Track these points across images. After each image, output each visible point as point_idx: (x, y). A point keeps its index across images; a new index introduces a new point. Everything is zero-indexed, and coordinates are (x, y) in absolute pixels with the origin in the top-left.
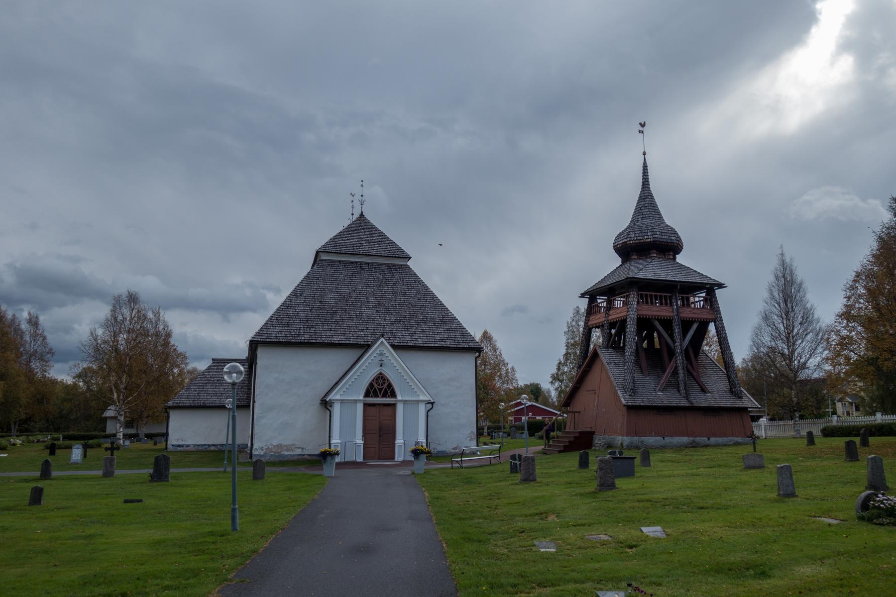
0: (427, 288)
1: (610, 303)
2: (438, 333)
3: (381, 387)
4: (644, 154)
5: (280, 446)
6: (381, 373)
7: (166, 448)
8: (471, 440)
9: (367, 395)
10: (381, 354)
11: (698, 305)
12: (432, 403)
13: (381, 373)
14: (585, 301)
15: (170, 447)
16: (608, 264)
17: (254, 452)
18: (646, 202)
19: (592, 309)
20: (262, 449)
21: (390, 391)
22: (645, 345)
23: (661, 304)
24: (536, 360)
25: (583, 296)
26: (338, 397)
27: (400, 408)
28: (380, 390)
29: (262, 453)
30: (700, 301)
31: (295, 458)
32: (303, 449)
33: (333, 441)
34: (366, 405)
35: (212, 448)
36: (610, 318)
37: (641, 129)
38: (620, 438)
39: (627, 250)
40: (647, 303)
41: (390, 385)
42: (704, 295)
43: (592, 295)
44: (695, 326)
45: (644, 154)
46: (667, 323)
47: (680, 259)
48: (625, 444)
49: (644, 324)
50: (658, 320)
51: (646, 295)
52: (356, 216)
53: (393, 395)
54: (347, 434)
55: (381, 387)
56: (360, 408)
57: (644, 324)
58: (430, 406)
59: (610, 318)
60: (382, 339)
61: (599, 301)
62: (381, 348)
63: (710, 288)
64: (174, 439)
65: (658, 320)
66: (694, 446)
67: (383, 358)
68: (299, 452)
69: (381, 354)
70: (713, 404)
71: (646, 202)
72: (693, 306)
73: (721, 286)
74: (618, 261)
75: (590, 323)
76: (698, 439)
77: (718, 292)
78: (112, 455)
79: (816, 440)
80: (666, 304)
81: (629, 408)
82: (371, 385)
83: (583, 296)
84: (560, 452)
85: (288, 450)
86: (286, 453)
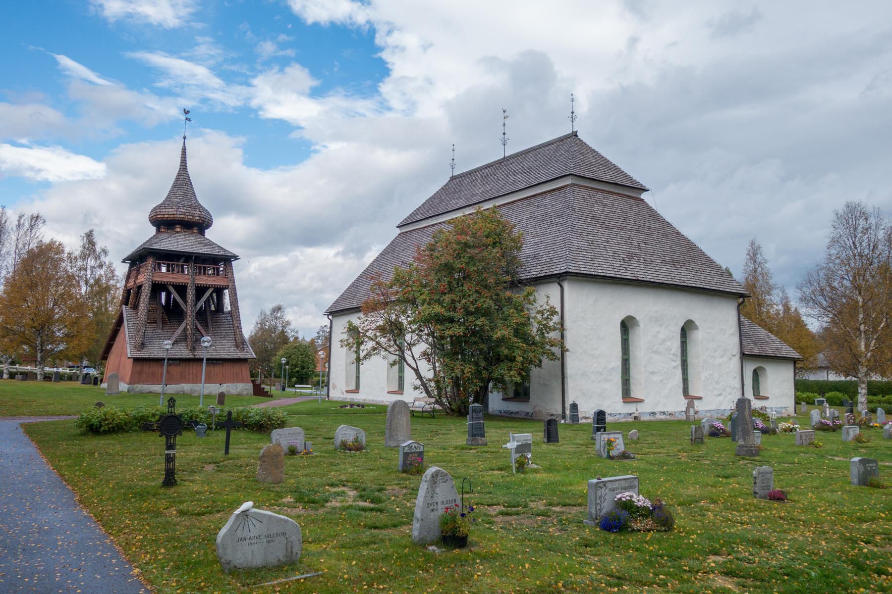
0: (361, 276)
16: (142, 233)
18: (183, 180)
25: (124, 261)
37: (188, 116)
39: (163, 223)
40: (200, 273)
46: (181, 289)
47: (209, 234)
49: (157, 288)
50: (173, 285)
56: (206, 385)
57: (157, 288)
63: (227, 259)
65: (173, 285)
70: (152, 356)
71: (183, 180)
73: (236, 258)
74: (153, 230)
79: (561, 433)
81: (136, 360)
83: (124, 261)
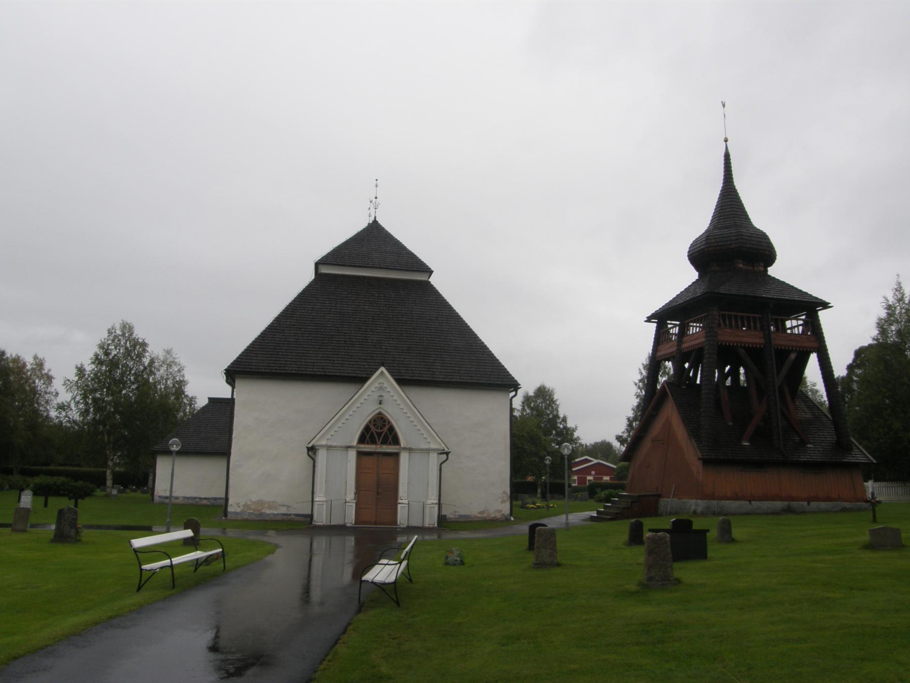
1: (683, 329)
2: (462, 362)
3: (379, 433)
4: (726, 141)
5: (261, 502)
6: (380, 413)
7: (153, 500)
8: (503, 502)
9: (362, 440)
10: (381, 388)
11: (796, 331)
12: (447, 454)
13: (380, 413)
14: (653, 326)
15: (156, 499)
17: (230, 509)
19: (661, 336)
20: (238, 504)
21: (391, 437)
22: (728, 382)
23: (749, 328)
24: (601, 398)
25: (649, 320)
26: (324, 442)
27: (404, 457)
28: (379, 434)
29: (239, 510)
30: (798, 326)
31: (279, 518)
32: (288, 507)
33: (316, 499)
34: (360, 454)
35: (204, 502)
36: (684, 346)
38: (693, 501)
41: (392, 429)
42: (803, 317)
43: (661, 317)
44: (793, 356)
45: (726, 141)
48: (699, 509)
50: (745, 348)
51: (730, 316)
52: (372, 219)
53: (396, 441)
54: (336, 490)
55: (379, 433)
56: (352, 455)
58: (445, 456)
59: (684, 346)
60: (382, 369)
61: (669, 326)
62: (381, 380)
64: (161, 487)
66: (789, 510)
67: (382, 392)
68: (283, 510)
69: (381, 388)
71: (730, 204)
72: (789, 331)
75: (659, 354)
76: (794, 504)
77: (823, 315)
78: (76, 505)
80: (755, 328)
82: (367, 428)
83: (649, 320)
84: (611, 519)
85: (270, 508)
86: (268, 512)
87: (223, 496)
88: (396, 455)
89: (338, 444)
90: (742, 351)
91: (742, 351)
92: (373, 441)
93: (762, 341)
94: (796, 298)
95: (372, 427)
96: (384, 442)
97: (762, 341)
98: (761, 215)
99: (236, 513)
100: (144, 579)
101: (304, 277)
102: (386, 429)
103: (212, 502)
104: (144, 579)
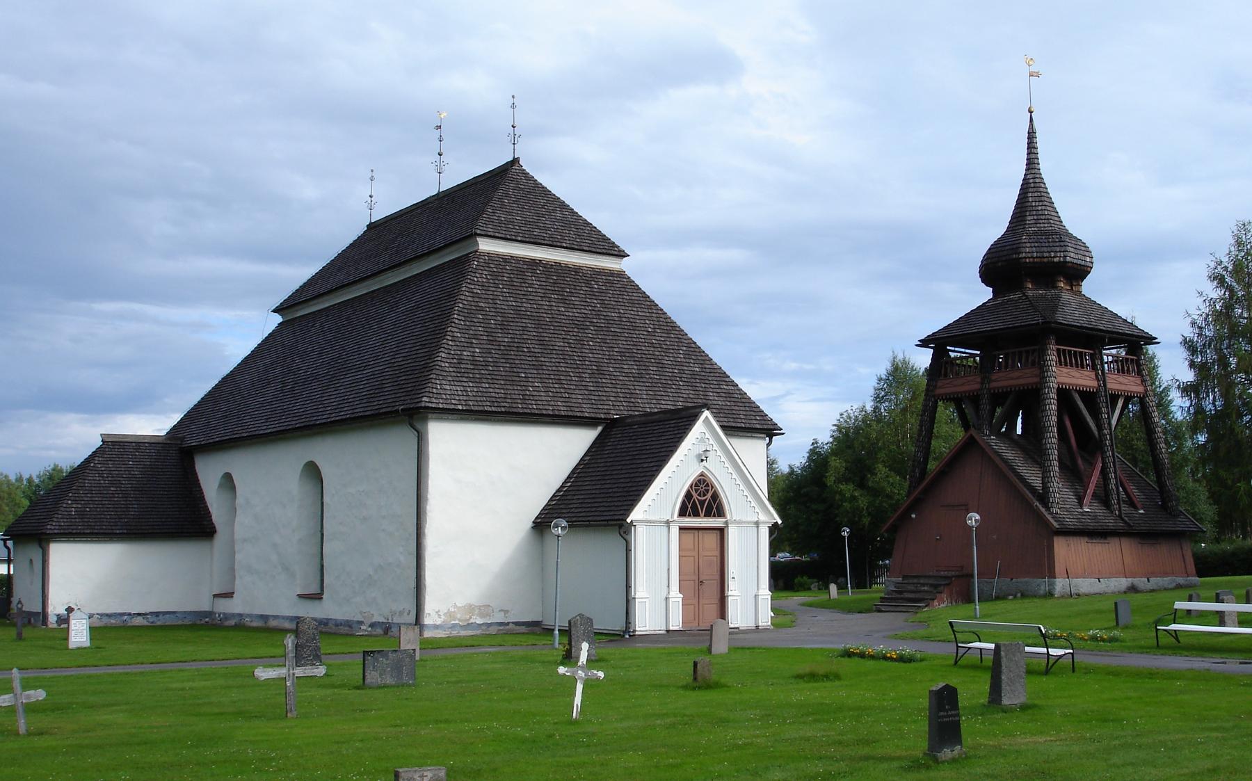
9: (683, 513)
17: (427, 621)
21: (714, 506)
25: (924, 343)
28: (702, 503)
32: (506, 612)
35: (139, 621)
41: (715, 496)
50: (1079, 392)
53: (720, 512)
82: (688, 495)
83: (924, 343)
87: (40, 610)
88: (721, 531)
89: (657, 518)
90: (1077, 396)
91: (1077, 396)
92: (696, 514)
93: (1095, 384)
94: (1136, 332)
95: (693, 493)
96: (708, 514)
97: (1095, 384)
98: (1076, 213)
99: (436, 627)
100: (1051, 662)
101: (359, 229)
102: (709, 496)
103: (106, 620)
104: (1051, 662)
